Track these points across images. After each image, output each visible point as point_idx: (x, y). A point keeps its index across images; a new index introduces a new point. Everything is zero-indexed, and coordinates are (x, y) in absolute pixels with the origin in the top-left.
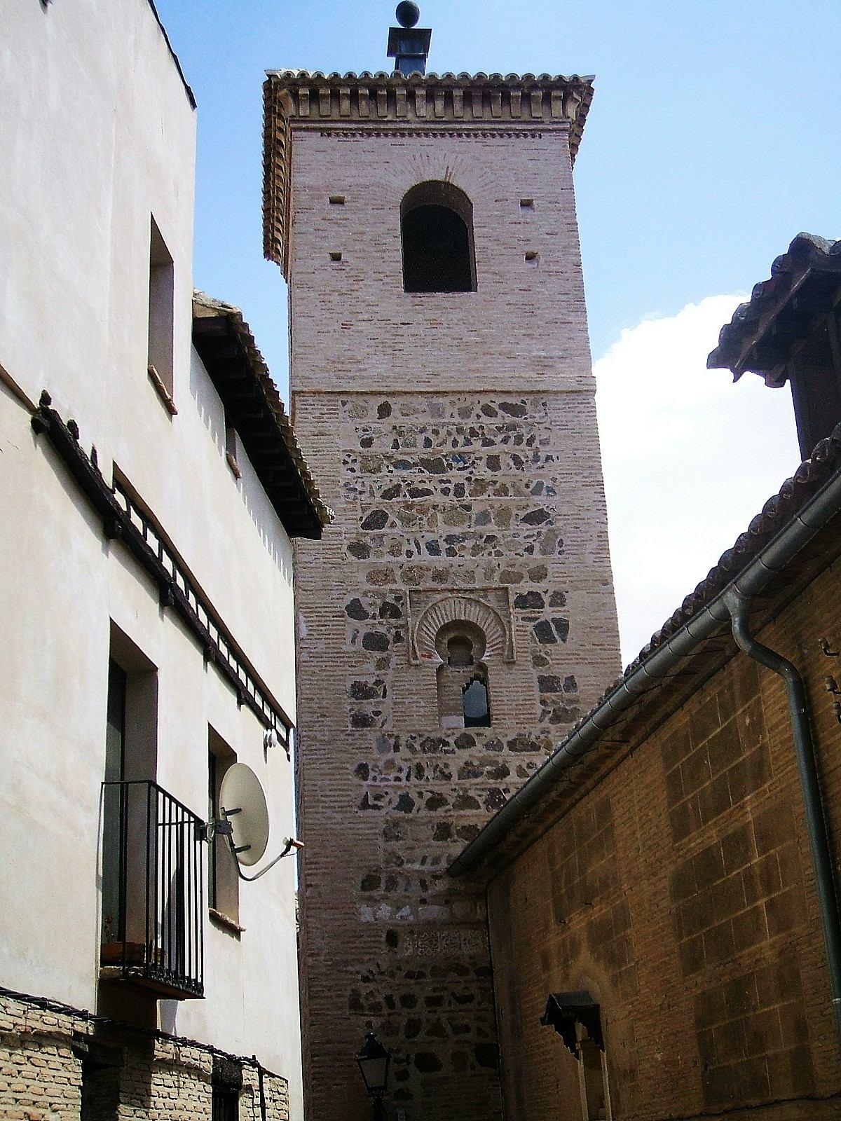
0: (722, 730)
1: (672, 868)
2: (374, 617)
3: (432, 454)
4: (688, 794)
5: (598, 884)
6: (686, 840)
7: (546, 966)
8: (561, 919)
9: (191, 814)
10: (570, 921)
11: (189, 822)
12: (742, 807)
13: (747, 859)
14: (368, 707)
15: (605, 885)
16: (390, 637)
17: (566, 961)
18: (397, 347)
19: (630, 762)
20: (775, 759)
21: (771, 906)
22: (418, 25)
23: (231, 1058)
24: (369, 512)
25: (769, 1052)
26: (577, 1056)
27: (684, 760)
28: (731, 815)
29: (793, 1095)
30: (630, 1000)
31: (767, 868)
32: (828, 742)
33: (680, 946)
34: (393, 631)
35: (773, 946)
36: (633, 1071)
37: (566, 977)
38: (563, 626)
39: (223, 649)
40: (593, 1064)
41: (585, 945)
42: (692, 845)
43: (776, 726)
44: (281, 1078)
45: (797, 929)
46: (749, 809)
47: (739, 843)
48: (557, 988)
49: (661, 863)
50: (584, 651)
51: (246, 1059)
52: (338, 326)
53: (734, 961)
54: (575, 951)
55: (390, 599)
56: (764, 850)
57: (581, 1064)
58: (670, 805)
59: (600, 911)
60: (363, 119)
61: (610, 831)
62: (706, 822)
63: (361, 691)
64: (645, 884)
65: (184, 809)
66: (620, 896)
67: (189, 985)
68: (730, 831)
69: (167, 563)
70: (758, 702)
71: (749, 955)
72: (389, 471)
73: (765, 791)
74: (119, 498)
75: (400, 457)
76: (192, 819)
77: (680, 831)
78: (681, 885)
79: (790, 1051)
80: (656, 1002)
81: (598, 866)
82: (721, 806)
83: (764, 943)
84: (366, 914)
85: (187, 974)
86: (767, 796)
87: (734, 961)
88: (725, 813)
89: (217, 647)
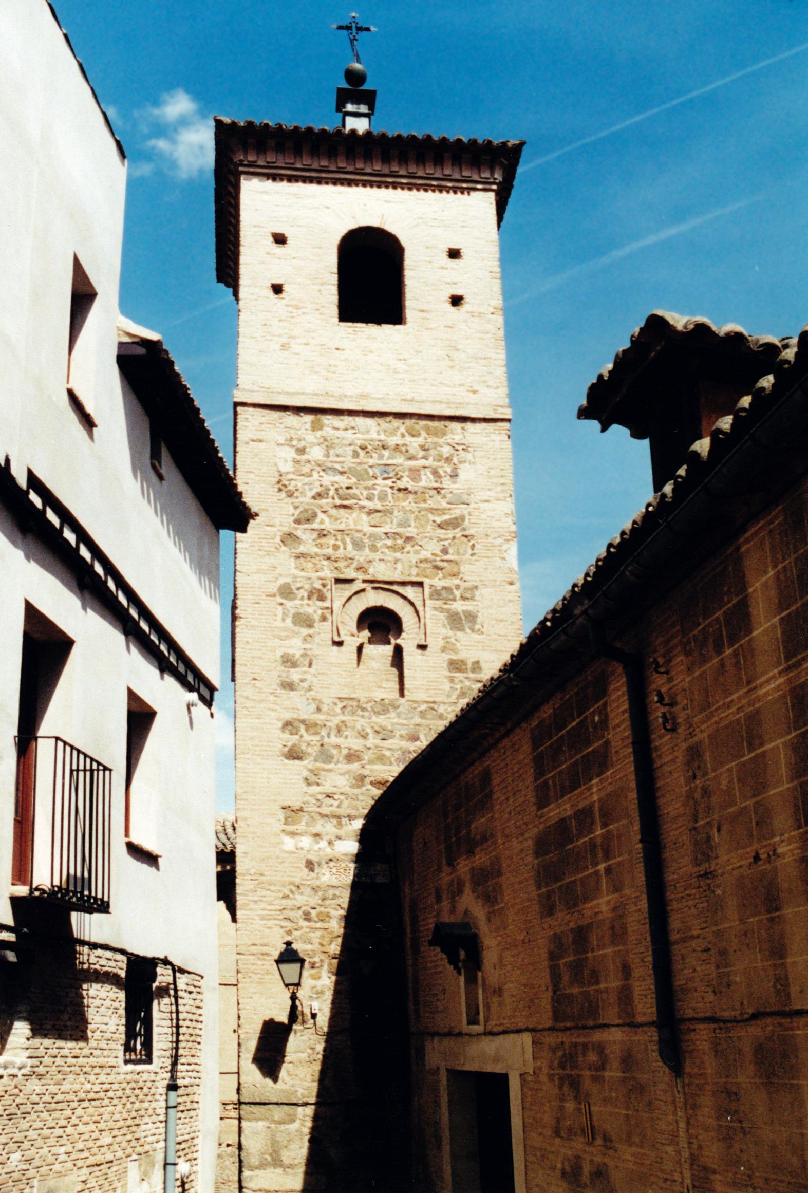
0: (578, 724)
1: (536, 830)
2: (302, 599)
3: (360, 464)
4: (550, 772)
5: (478, 837)
6: (546, 810)
7: (439, 899)
8: (450, 864)
9: (99, 764)
10: (458, 864)
11: (98, 770)
12: (590, 789)
13: (591, 831)
14: (295, 675)
15: (484, 839)
16: (317, 617)
17: (453, 897)
18: (332, 369)
19: (506, 742)
20: (616, 752)
21: (608, 870)
22: (366, 87)
23: (144, 959)
24: (301, 509)
25: (603, 986)
26: (459, 973)
27: (547, 744)
28: (582, 793)
29: (617, 1021)
30: (500, 933)
31: (607, 837)
32: (657, 744)
33: (539, 895)
34: (320, 612)
35: (608, 902)
36: (500, 989)
37: (453, 910)
38: (471, 617)
39: (144, 626)
40: (471, 981)
41: (468, 884)
42: (552, 814)
43: (618, 726)
44: (197, 974)
45: (627, 892)
46: (595, 790)
47: (584, 816)
48: (446, 918)
49: (527, 826)
50: (489, 640)
51: (158, 959)
52: (278, 347)
53: (579, 912)
54: (460, 892)
55: (318, 585)
56: (605, 825)
57: (462, 979)
58: (536, 780)
59: (481, 859)
60: (306, 167)
61: (489, 796)
62: (562, 796)
63: (289, 661)
64: (515, 841)
65: (92, 760)
66: (494, 850)
67: (96, 902)
68: (580, 807)
69: (85, 553)
70: (605, 704)
71: (591, 908)
72: (320, 476)
73: (607, 778)
74: (35, 498)
75: (330, 465)
76: (101, 768)
77: (542, 802)
78: (541, 846)
79: (617, 987)
80: (520, 937)
81: (479, 823)
82: (575, 786)
83: (601, 901)
84: (289, 843)
85: (93, 894)
86: (609, 781)
87: (579, 912)
88: (576, 792)
89: (137, 624)
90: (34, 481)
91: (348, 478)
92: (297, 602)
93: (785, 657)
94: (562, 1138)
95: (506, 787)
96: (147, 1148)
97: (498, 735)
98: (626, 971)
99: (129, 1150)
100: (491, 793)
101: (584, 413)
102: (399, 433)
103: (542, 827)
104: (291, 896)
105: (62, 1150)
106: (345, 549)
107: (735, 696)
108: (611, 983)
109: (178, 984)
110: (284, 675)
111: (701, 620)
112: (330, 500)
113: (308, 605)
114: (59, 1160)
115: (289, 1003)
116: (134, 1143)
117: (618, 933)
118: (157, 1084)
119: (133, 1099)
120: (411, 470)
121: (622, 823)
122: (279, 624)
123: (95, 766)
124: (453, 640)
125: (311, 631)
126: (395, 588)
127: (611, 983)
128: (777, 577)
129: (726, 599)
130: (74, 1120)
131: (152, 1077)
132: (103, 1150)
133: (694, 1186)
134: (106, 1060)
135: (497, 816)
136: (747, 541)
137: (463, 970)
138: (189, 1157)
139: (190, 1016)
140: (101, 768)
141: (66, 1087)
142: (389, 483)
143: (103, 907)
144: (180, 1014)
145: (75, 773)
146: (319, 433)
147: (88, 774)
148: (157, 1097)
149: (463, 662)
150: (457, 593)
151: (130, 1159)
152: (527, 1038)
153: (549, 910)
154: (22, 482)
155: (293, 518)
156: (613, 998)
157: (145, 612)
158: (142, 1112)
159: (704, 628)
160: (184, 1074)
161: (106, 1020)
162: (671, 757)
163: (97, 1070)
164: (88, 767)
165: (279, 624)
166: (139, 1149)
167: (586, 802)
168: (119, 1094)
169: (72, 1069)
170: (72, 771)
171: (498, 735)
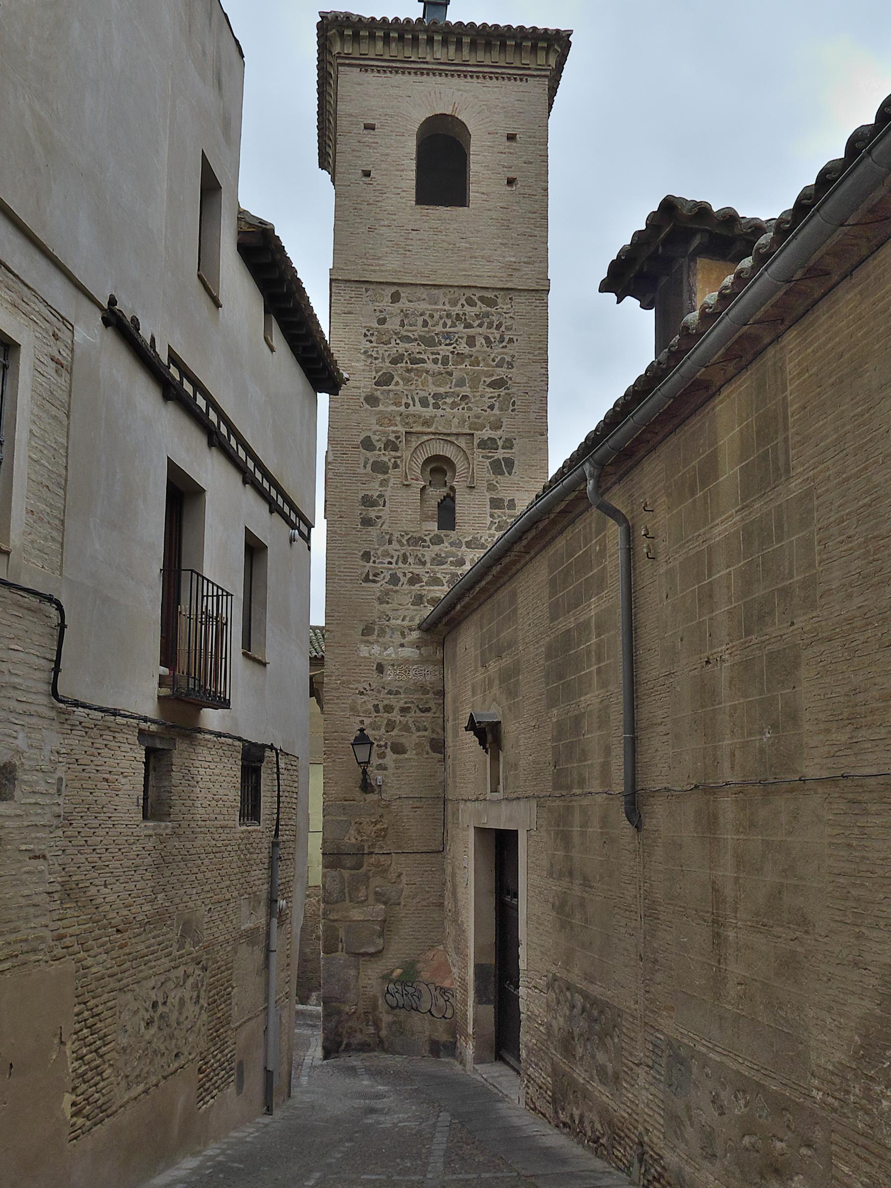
1: (548, 639)
2: (380, 450)
11: (222, 595)
12: (589, 605)
14: (372, 513)
15: (509, 646)
21: (599, 671)
23: (255, 745)
26: (487, 752)
31: (599, 646)
34: (393, 460)
43: (613, 554)
45: (611, 688)
56: (598, 635)
63: (368, 502)
65: (218, 587)
75: (405, 334)
76: (225, 594)
90: (174, 358)
91: (418, 344)
92: (377, 452)
93: (742, 499)
94: (554, 878)
95: (528, 604)
96: (255, 889)
97: (523, 562)
98: (607, 750)
99: (242, 891)
100: (516, 609)
101: (605, 287)
102: (459, 305)
103: (553, 636)
104: (365, 692)
105: (194, 891)
106: (414, 406)
107: (702, 530)
108: (596, 760)
109: (280, 764)
110: (364, 513)
111: (681, 468)
112: (403, 365)
113: (384, 454)
114: (192, 899)
115: (361, 776)
116: (245, 885)
117: (603, 722)
118: (263, 840)
119: (245, 852)
120: (468, 337)
121: (612, 633)
122: (362, 471)
123: (220, 592)
124: (494, 482)
125: (386, 477)
126: (452, 439)
127: (596, 760)
128: (741, 431)
129: (701, 451)
130: (203, 868)
131: (260, 835)
132: (223, 891)
133: (645, 915)
134: (227, 822)
135: (520, 627)
136: (721, 402)
137: (489, 750)
138: (286, 895)
139: (288, 789)
140: (225, 594)
141: (198, 843)
142: (450, 348)
143: (224, 704)
144: (281, 798)
145: (205, 598)
146: (396, 305)
147: (215, 598)
148: (263, 850)
149: (502, 500)
150: (500, 443)
151: (243, 898)
152: (534, 804)
153: (552, 703)
154: (164, 358)
155: (374, 381)
156: (596, 772)
157: (259, 464)
158: (252, 862)
159: (683, 475)
160: (283, 833)
161: (227, 792)
162: (651, 580)
163: (221, 831)
164: (215, 594)
165: (362, 471)
166: (249, 890)
167: (587, 616)
168: (236, 848)
169: (202, 829)
170: (203, 596)
171: (523, 562)
